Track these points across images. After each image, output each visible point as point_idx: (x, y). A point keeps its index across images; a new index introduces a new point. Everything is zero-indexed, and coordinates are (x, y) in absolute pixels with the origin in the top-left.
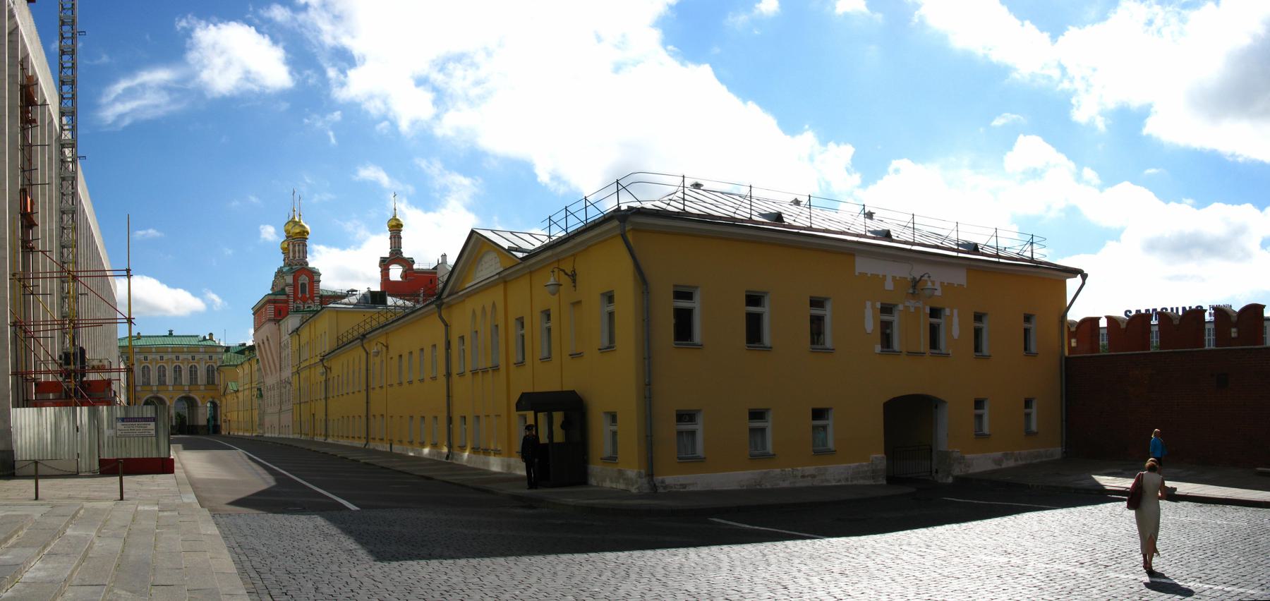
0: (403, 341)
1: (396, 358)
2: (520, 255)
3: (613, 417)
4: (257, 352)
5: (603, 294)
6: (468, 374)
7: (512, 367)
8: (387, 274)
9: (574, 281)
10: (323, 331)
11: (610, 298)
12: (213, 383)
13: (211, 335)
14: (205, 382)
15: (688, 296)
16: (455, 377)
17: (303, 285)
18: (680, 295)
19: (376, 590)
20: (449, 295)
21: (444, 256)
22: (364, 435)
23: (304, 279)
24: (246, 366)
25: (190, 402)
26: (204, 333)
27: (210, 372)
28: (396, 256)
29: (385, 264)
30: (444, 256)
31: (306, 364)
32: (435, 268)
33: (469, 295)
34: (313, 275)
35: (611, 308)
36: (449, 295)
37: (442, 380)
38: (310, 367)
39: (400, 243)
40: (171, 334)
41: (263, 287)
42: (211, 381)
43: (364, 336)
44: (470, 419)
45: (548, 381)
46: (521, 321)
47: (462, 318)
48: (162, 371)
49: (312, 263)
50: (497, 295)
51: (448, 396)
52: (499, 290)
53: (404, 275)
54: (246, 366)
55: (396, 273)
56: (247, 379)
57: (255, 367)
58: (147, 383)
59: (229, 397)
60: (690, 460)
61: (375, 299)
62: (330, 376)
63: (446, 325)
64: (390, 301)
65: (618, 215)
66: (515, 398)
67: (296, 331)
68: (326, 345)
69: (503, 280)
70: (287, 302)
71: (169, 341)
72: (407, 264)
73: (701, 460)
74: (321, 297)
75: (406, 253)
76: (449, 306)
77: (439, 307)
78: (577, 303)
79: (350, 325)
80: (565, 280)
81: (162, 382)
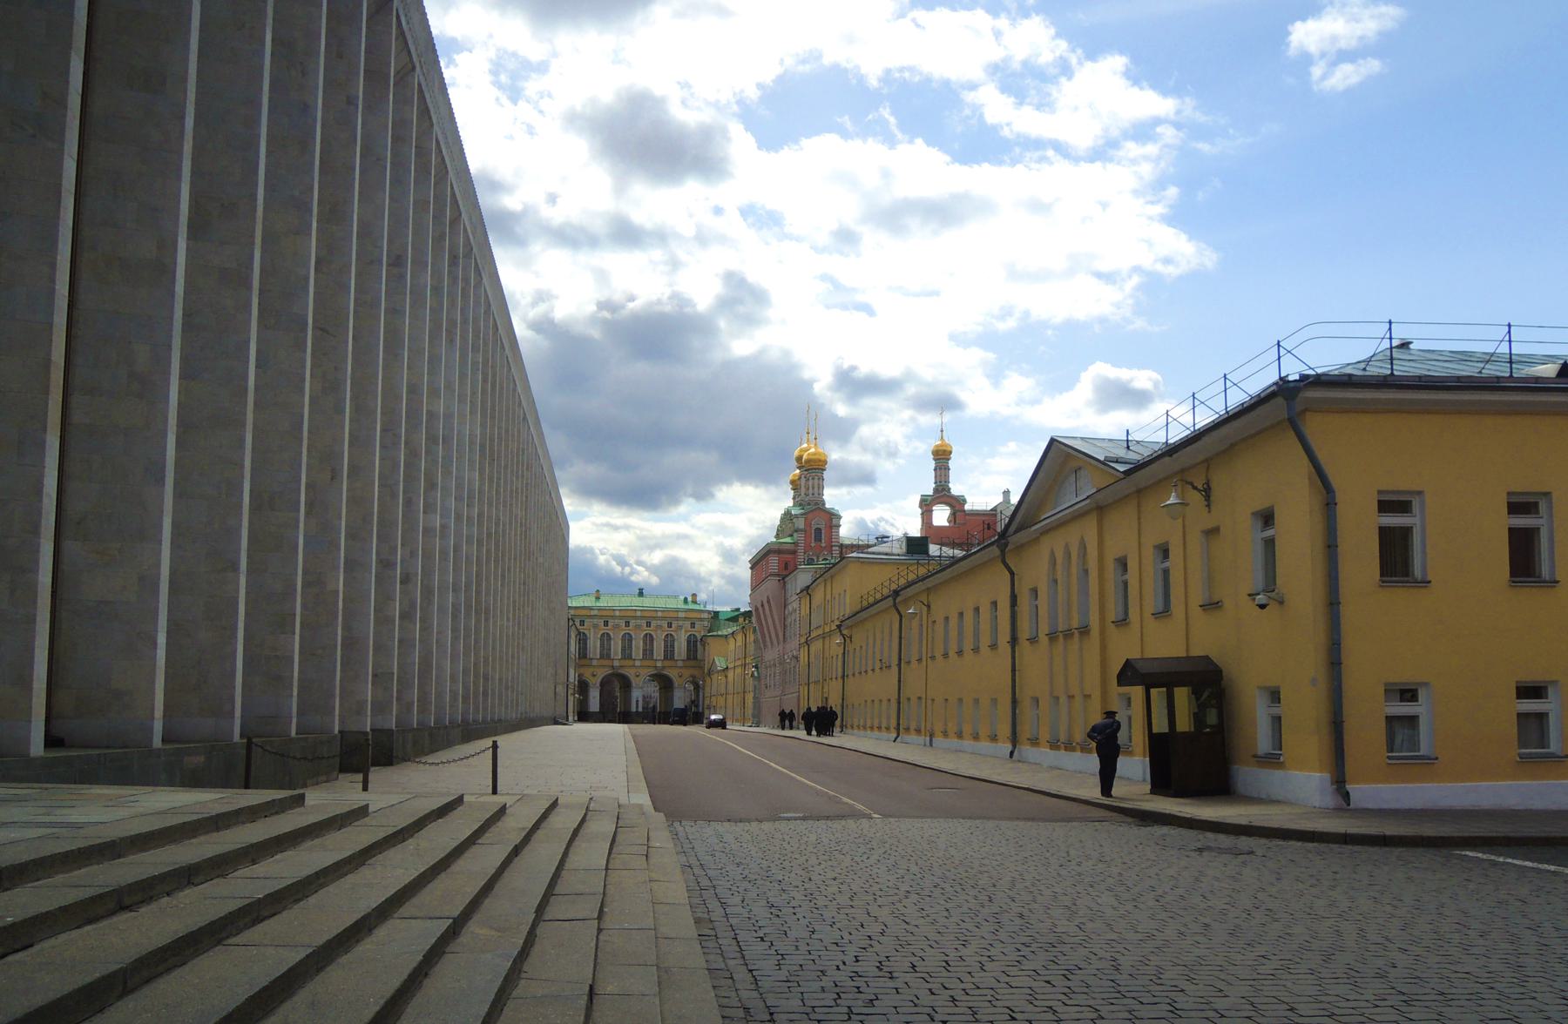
0: (948, 603)
1: (940, 621)
2: (1122, 468)
3: (1275, 696)
4: (754, 619)
5: (1255, 514)
9: (1208, 497)
13: (694, 595)
14: (684, 655)
15: (1403, 507)
16: (1024, 645)
17: (818, 531)
19: (910, 938)
20: (1016, 532)
21: (1007, 493)
22: (893, 723)
25: (665, 683)
27: (693, 644)
28: (942, 493)
29: (926, 505)
30: (1007, 493)
31: (820, 632)
32: (994, 509)
33: (1047, 531)
34: (832, 519)
35: (1269, 533)
38: (823, 637)
39: (947, 476)
43: (896, 593)
45: (1163, 643)
46: (1123, 564)
47: (1035, 568)
48: (628, 639)
50: (1089, 529)
51: (1014, 670)
53: (953, 517)
55: (941, 516)
57: (751, 638)
58: (606, 655)
59: (715, 677)
60: (1424, 765)
61: (916, 546)
62: (850, 648)
63: (1012, 574)
64: (934, 549)
65: (1284, 390)
66: (1116, 667)
68: (848, 605)
69: (1099, 509)
70: (794, 552)
72: (956, 504)
73: (1431, 760)
74: (842, 546)
75: (956, 489)
76: (1020, 547)
79: (876, 582)
80: (1196, 498)
81: (627, 654)
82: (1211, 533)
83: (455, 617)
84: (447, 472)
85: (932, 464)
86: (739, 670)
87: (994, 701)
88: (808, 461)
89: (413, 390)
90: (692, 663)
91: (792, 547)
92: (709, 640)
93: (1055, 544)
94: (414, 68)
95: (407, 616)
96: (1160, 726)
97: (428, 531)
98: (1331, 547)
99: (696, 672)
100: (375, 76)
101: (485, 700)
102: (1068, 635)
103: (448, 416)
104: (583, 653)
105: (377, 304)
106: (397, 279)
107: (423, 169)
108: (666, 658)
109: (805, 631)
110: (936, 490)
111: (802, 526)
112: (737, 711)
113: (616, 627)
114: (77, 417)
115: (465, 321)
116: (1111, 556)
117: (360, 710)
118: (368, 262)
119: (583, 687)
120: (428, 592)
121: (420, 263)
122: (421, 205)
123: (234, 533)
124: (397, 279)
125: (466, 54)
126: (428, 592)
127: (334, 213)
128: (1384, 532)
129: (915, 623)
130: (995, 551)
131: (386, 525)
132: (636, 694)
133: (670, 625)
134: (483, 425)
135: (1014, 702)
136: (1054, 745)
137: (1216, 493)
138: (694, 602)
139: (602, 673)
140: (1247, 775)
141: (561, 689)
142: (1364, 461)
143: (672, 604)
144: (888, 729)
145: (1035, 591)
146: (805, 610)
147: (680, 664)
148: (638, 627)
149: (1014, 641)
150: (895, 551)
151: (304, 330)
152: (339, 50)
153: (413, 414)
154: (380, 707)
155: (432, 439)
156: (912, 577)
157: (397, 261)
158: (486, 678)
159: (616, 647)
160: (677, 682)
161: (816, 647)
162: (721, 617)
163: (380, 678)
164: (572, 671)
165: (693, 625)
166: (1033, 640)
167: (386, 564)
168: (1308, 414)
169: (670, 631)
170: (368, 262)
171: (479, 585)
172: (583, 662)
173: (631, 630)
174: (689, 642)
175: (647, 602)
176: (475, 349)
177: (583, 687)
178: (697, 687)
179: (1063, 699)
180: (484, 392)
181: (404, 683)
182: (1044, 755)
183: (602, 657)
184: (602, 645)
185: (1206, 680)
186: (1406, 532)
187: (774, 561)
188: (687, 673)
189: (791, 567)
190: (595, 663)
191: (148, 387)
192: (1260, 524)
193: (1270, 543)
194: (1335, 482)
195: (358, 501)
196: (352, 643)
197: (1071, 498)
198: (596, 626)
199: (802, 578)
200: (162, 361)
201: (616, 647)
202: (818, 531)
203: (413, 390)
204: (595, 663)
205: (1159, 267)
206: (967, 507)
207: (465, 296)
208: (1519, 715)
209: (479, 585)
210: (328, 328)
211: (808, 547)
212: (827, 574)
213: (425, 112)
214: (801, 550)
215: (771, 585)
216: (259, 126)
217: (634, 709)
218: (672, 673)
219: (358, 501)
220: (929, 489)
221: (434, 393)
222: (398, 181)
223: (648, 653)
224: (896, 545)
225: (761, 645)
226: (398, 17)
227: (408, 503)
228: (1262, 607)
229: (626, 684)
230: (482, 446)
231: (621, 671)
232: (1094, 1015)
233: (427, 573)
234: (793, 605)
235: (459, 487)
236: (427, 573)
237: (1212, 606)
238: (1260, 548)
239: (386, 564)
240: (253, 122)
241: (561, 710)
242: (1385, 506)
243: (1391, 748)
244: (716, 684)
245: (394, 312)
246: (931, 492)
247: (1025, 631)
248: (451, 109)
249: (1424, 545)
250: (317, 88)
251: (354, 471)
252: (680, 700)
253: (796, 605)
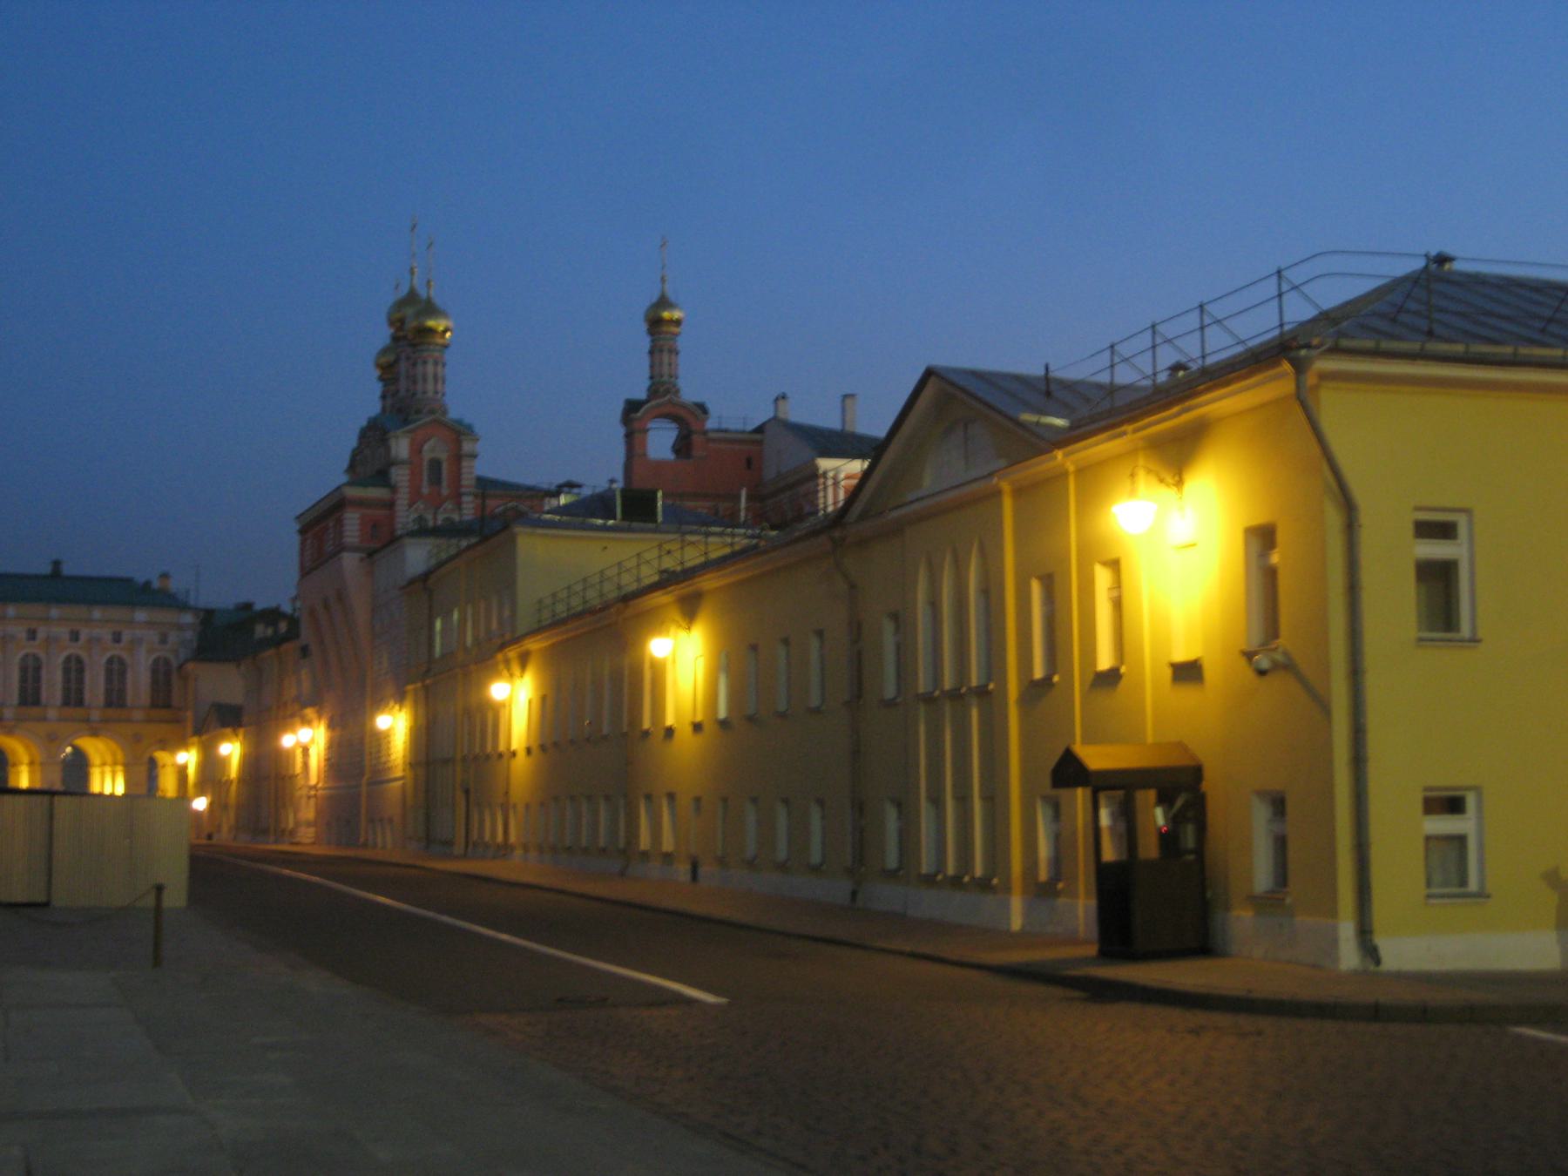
15: (1445, 531)
17: (435, 465)
20: (863, 516)
28: (661, 387)
32: (760, 430)
36: (863, 516)
53: (683, 447)
55: (660, 441)
70: (390, 505)
72: (689, 420)
75: (689, 391)
96: (1109, 854)
110: (654, 392)
125: (462, 389)
140: (1240, 921)
169: (116, 651)
174: (154, 671)
202: (435, 465)
205: (1401, 833)
206: (711, 424)
208: (1428, 839)
228: (1262, 673)
243: (1429, 884)
249: (1473, 592)
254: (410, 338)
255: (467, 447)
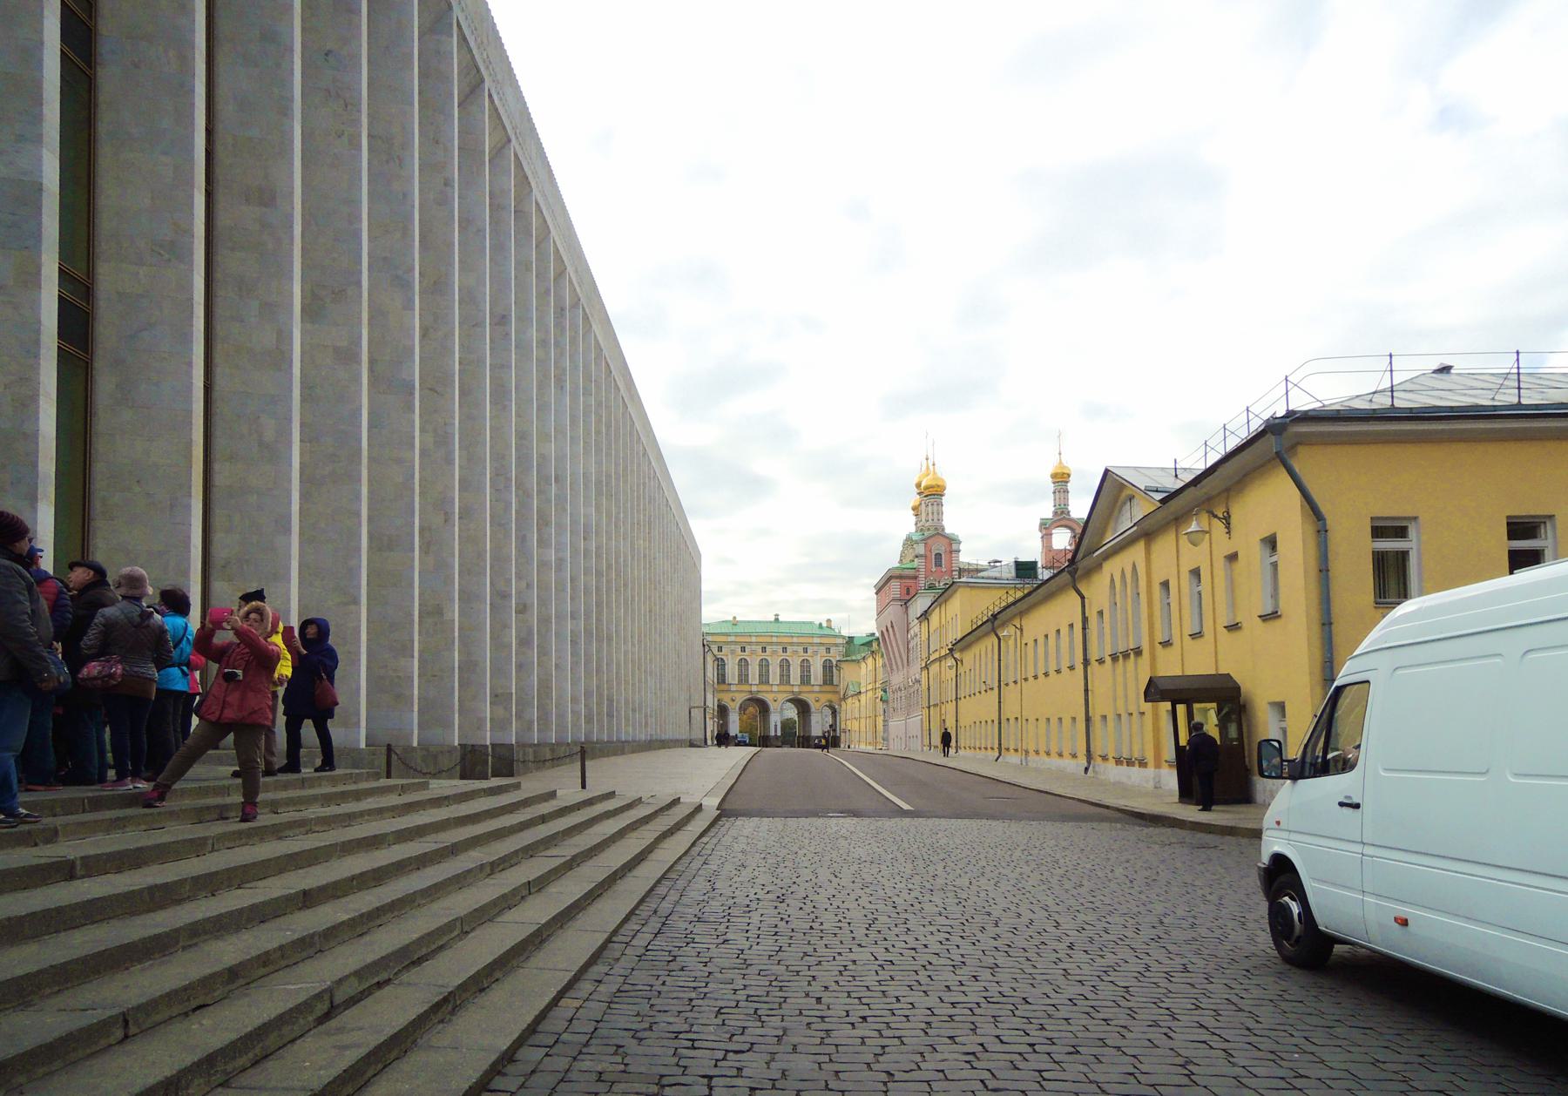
1: (1031, 644)
3: (1280, 707)
5: (1264, 540)
6: (1108, 660)
7: (1187, 639)
8: (1050, 541)
9: (1228, 525)
10: (959, 614)
11: (1271, 543)
12: (831, 683)
15: (1401, 532)
16: (1094, 664)
18: (1380, 530)
23: (939, 546)
24: (870, 661)
25: (803, 707)
26: (820, 618)
27: (828, 668)
29: (1046, 528)
31: (936, 655)
33: (1107, 556)
34: (952, 543)
35: (1274, 559)
37: (1080, 668)
38: (940, 659)
40: (777, 620)
41: (890, 556)
42: (828, 679)
43: (995, 616)
44: (1110, 717)
45: (1195, 662)
48: (764, 665)
49: (950, 528)
50: (1137, 553)
51: (1086, 690)
52: (1140, 547)
54: (870, 661)
56: (870, 678)
58: (744, 678)
63: (1083, 598)
65: (1273, 428)
67: (925, 616)
70: (916, 578)
71: (773, 628)
77: (1073, 574)
78: (1233, 557)
80: (1219, 526)
81: (764, 679)
82: (1233, 557)
83: (574, 643)
84: (561, 509)
85: (1051, 487)
86: (870, 694)
87: (1074, 719)
88: (927, 488)
89: (522, 436)
90: (828, 688)
91: (912, 572)
92: (843, 665)
93: (1112, 567)
94: (509, 141)
95: (524, 642)
97: (543, 565)
98: (1324, 570)
99: (830, 696)
100: (470, 151)
101: (610, 723)
102: (1126, 656)
103: (560, 458)
104: (722, 679)
105: (482, 361)
106: (499, 342)
107: (524, 230)
108: (761, 682)
109: (925, 655)
110: (1055, 513)
111: (922, 551)
112: (870, 735)
113: (753, 652)
114: (219, 480)
115: (575, 368)
116: (1157, 579)
117: (480, 724)
118: (471, 324)
119: (723, 711)
120: (544, 621)
121: (523, 319)
122: (523, 266)
123: (353, 573)
124: (499, 342)
126: (544, 621)
127: (436, 287)
128: (1380, 559)
129: (1011, 642)
130: (1066, 577)
131: (500, 560)
132: (775, 720)
133: (806, 650)
134: (599, 463)
135: (1088, 719)
136: (1118, 761)
137: (1233, 520)
138: (829, 627)
139: (741, 698)
141: (697, 714)
142: (1357, 490)
143: (806, 630)
144: (1074, 756)
145: (1101, 613)
146: (924, 636)
147: (817, 689)
148: (774, 652)
149: (1086, 662)
150: (1005, 575)
151: (412, 394)
152: (434, 138)
153: (523, 460)
154: (500, 724)
155: (544, 479)
156: (1011, 600)
157: (501, 320)
158: (610, 700)
159: (754, 672)
160: (772, 706)
161: (934, 668)
162: (856, 642)
163: (499, 698)
164: (709, 696)
165: (828, 650)
166: (1101, 661)
167: (501, 595)
168: (1301, 450)
170: (471, 324)
171: (599, 613)
172: (723, 687)
173: (767, 656)
174: (824, 667)
175: (738, 630)
176: (587, 393)
177: (723, 711)
178: (834, 712)
179: (1124, 717)
180: (598, 433)
181: (523, 703)
182: (968, 753)
183: (740, 682)
184: (740, 670)
185: (1227, 695)
186: (1403, 556)
187: (895, 588)
188: (824, 698)
189: (912, 592)
190: (733, 688)
191: (274, 453)
192: (1268, 551)
193: (1275, 565)
194: (1324, 508)
195: (471, 539)
196: (470, 667)
197: (1126, 522)
198: (733, 652)
199: (920, 604)
200: (284, 433)
201: (754, 672)
202: (938, 556)
203: (522, 436)
204: (733, 688)
207: (573, 341)
209: (599, 613)
210: (435, 386)
211: (928, 573)
212: (944, 595)
213: (523, 181)
214: (922, 576)
215: (894, 610)
216: (360, 221)
217: (772, 733)
218: (768, 698)
219: (471, 539)
220: (1047, 511)
221: (544, 437)
222: (499, 248)
223: (785, 678)
224: (1005, 570)
225: (889, 667)
226: (490, 96)
227: (522, 539)
229: (763, 707)
230: (598, 482)
231: (760, 696)
232: (1404, 1087)
233: (543, 603)
234: (915, 629)
235: (574, 522)
236: (543, 603)
237: (1234, 627)
238: (1269, 569)
239: (501, 595)
240: (355, 217)
241: (697, 735)
242: (1378, 532)
244: (849, 708)
245: (500, 367)
246: (1050, 515)
247: (1094, 655)
248: (550, 171)
250: (413, 177)
251: (466, 513)
252: (818, 725)
253: (916, 629)
254: (932, 495)
255: (954, 547)
